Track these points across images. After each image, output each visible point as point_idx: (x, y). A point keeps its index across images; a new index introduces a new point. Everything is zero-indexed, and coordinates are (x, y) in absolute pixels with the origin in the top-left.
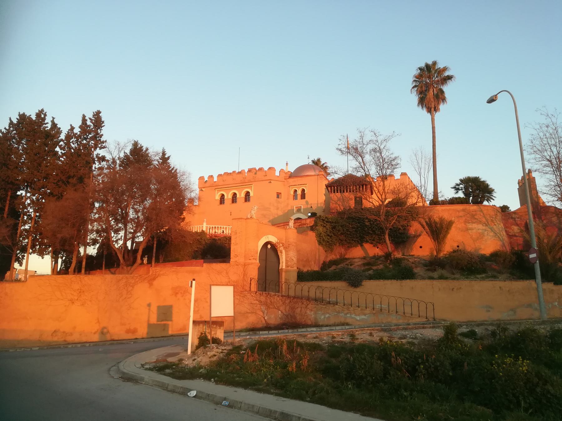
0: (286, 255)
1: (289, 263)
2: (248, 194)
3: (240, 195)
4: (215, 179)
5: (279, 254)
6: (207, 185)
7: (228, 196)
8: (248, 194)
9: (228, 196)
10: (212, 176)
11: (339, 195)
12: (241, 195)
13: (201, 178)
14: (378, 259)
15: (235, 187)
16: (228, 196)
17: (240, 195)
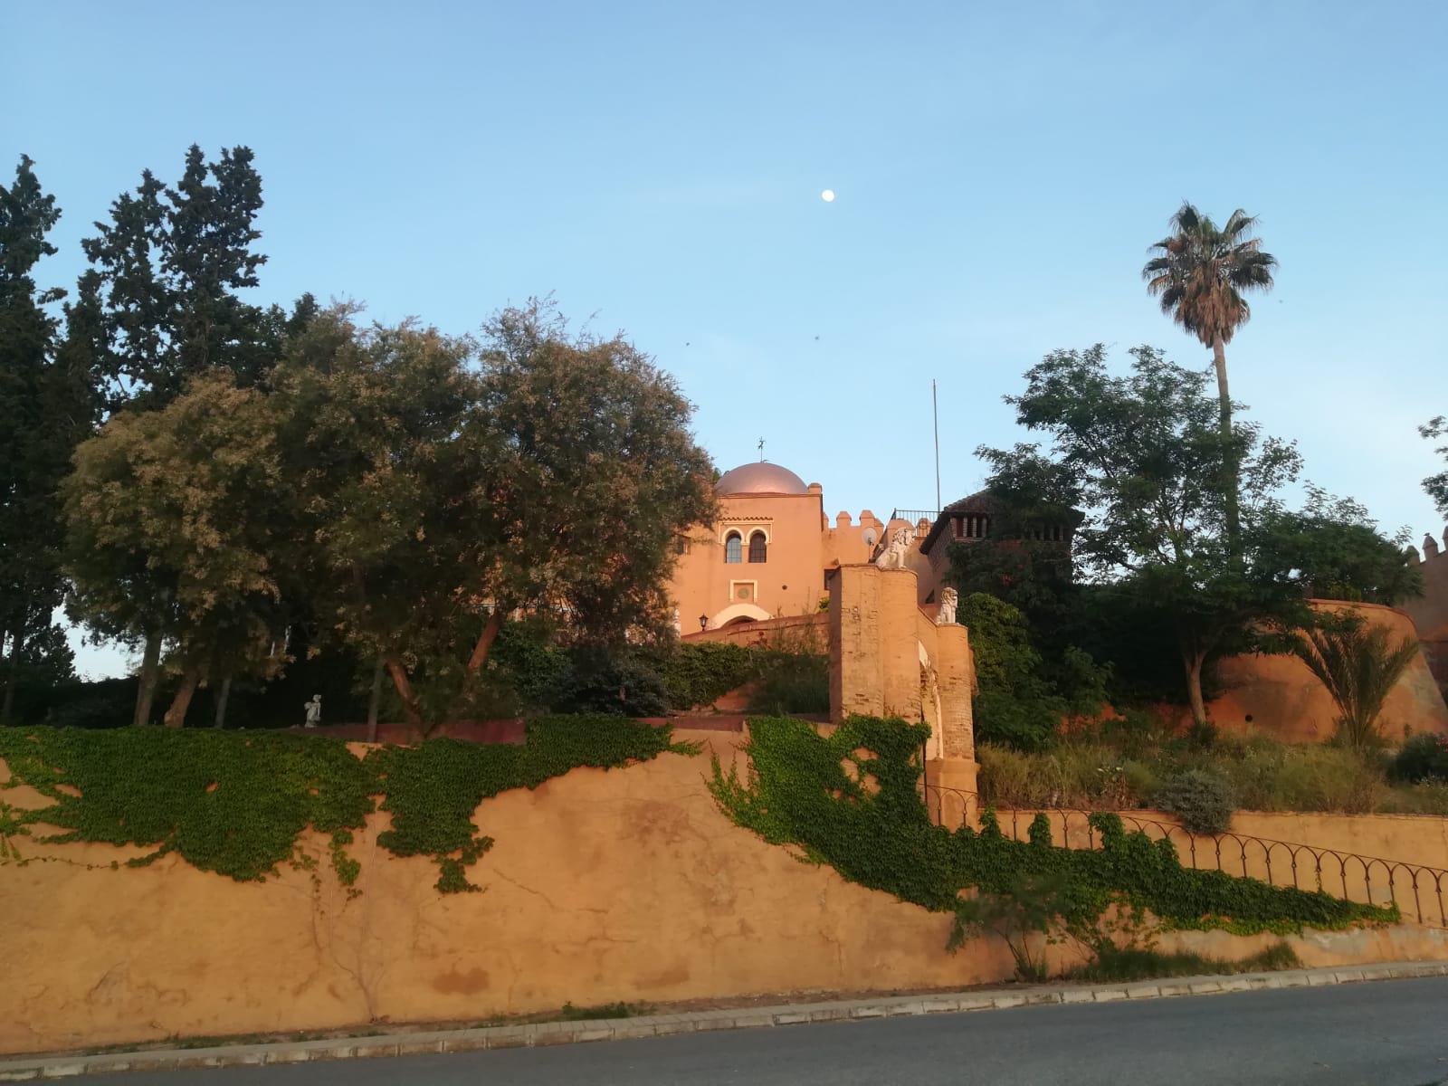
1: (958, 743)
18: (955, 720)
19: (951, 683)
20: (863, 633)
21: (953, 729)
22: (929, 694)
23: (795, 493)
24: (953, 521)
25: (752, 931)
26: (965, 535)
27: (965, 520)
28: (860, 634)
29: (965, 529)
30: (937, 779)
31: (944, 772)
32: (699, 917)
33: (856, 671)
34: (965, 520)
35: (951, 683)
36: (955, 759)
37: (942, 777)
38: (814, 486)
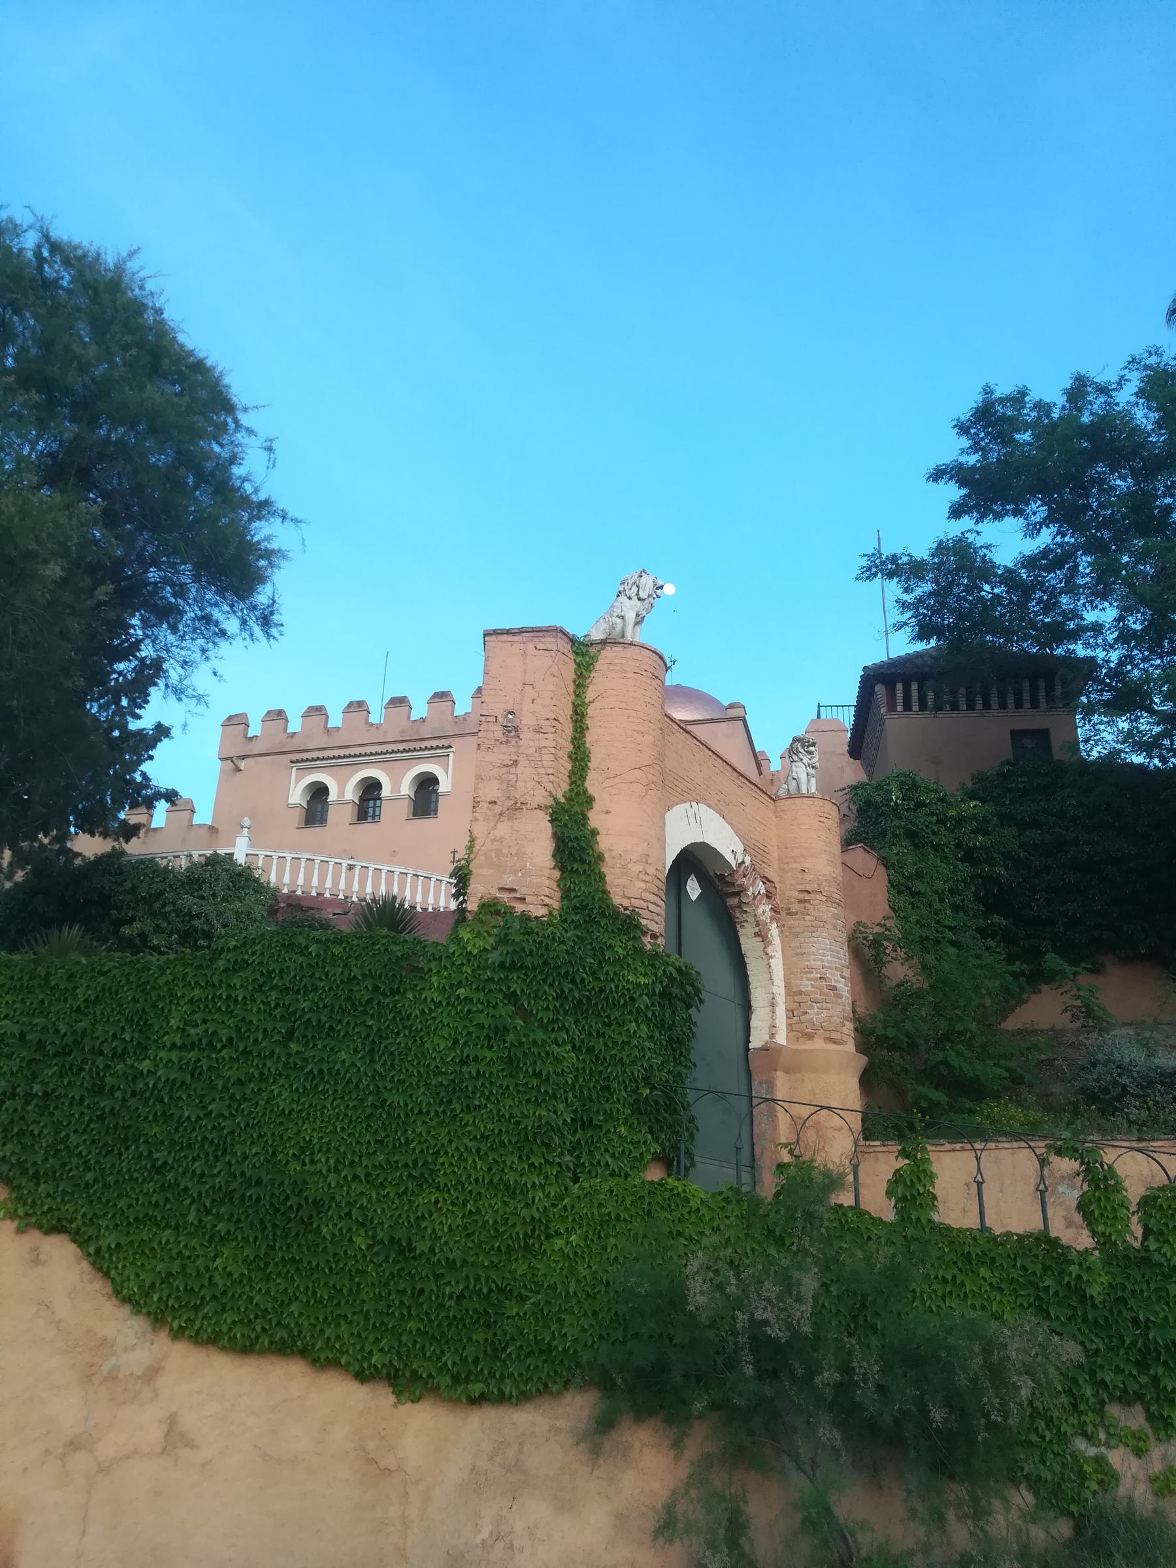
0: (793, 955)
1: (814, 1014)
2: (427, 783)
3: (396, 786)
4: (295, 725)
5: (749, 944)
6: (256, 748)
7: (341, 793)
8: (427, 783)
9: (341, 793)
10: (280, 714)
11: (119, 954)
12: (398, 785)
13: (237, 721)
14: (498, 913)
15: (378, 757)
16: (343, 790)
17: (396, 786)
18: (810, 969)
19: (801, 901)
20: (523, 762)
21: (806, 986)
22: (751, 919)
23: (709, 717)
24: (880, 689)
25: (190, 1444)
26: (899, 708)
27: (899, 686)
28: (515, 763)
29: (900, 701)
30: (771, 1085)
31: (787, 1071)
32: (68, 1410)
33: (501, 840)
34: (899, 686)
35: (801, 901)
36: (808, 1046)
37: (781, 1079)
38: (732, 706)
